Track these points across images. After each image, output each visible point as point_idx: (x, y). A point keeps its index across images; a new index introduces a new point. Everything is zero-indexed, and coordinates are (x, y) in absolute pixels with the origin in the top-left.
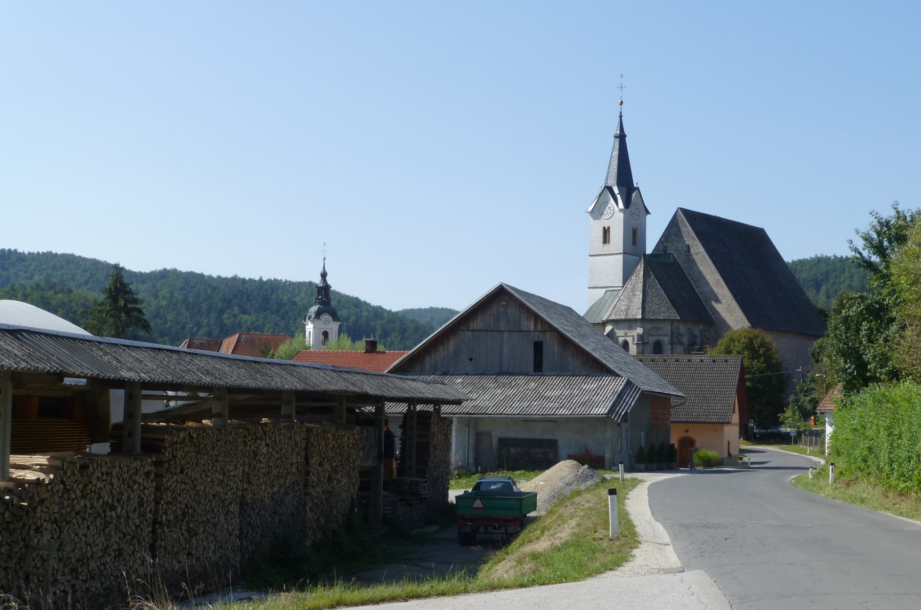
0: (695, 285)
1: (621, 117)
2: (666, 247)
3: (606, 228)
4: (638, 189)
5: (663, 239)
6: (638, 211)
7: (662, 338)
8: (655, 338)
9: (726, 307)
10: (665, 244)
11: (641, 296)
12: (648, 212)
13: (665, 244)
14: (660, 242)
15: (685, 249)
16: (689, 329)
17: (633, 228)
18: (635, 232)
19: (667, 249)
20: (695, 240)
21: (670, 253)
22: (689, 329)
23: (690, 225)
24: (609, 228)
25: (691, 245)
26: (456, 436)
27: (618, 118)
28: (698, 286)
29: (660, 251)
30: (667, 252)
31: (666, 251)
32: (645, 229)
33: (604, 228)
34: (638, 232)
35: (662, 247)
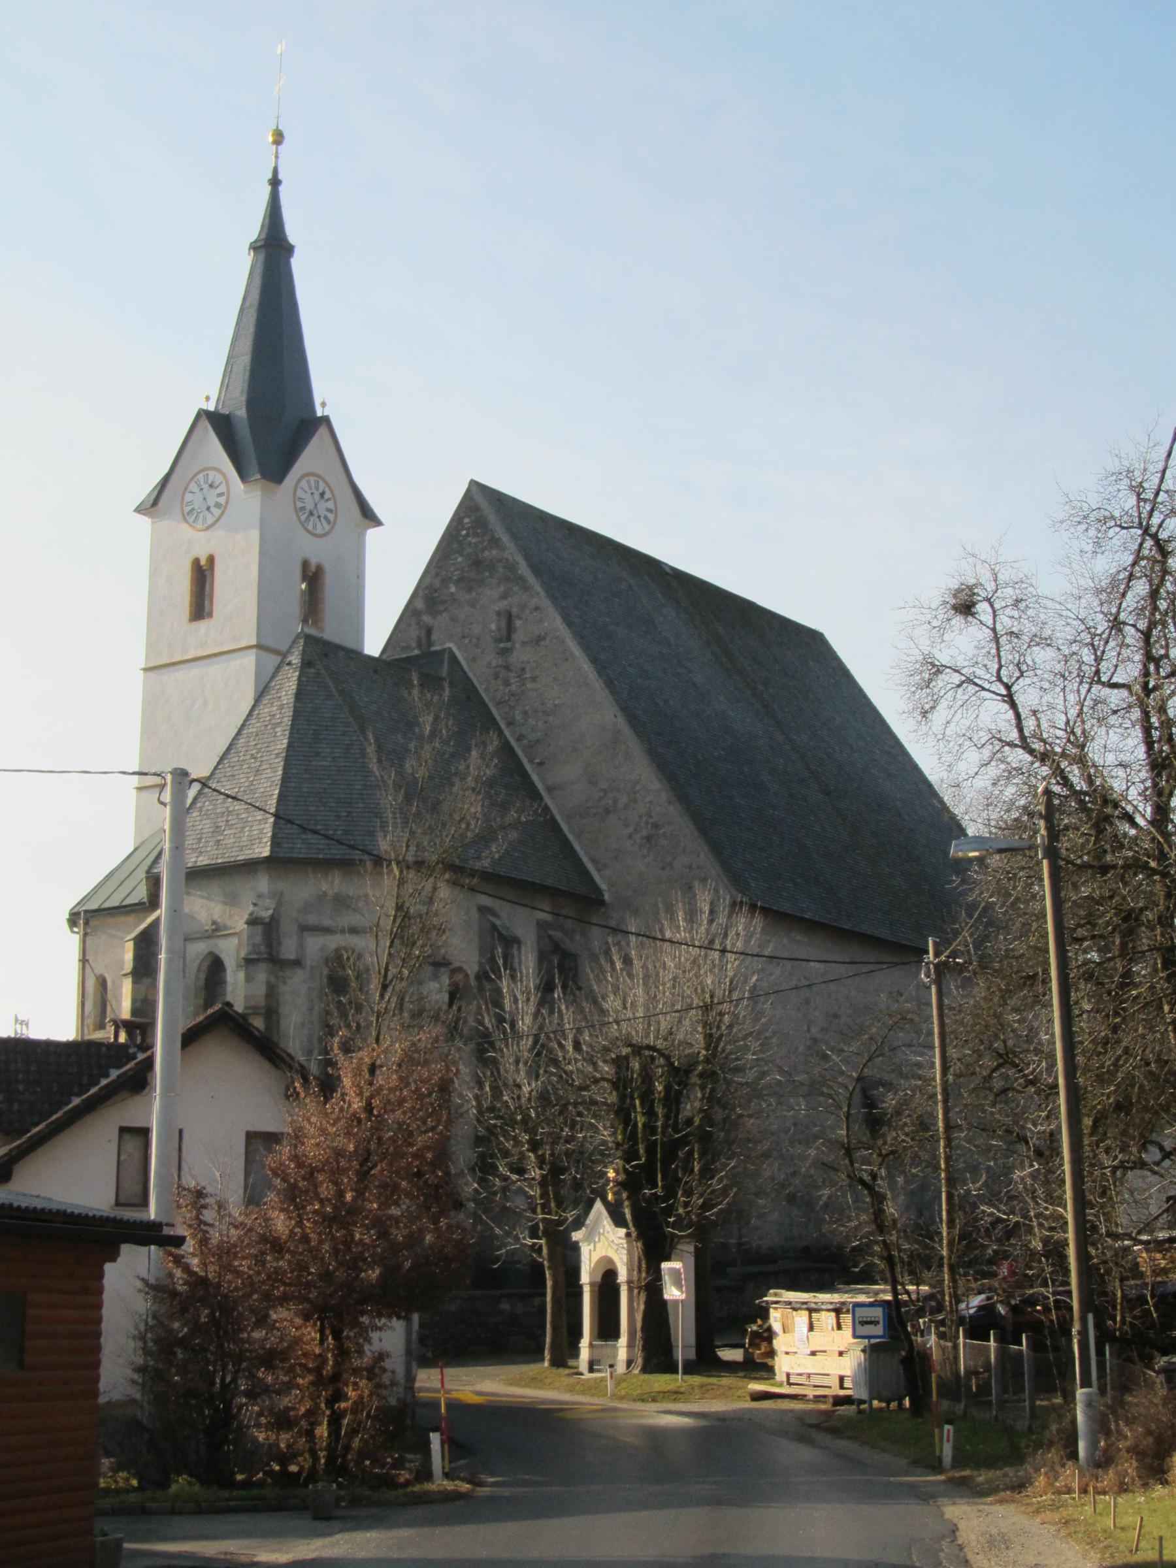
0: (531, 761)
1: (275, 182)
2: (429, 631)
3: (203, 562)
4: (326, 420)
5: (420, 604)
6: (331, 505)
7: (358, 942)
8: (333, 942)
9: (645, 833)
10: (426, 619)
11: (280, 773)
12: (369, 516)
13: (426, 619)
14: (410, 613)
15: (493, 627)
16: (482, 909)
17: (305, 564)
18: (313, 577)
19: (434, 637)
20: (525, 587)
21: (442, 652)
22: (482, 909)
23: (586, 648)
24: (211, 560)
25: (514, 610)
26: (792, 1411)
27: (268, 189)
28: (541, 764)
29: (408, 648)
30: (433, 649)
31: (430, 643)
32: (360, 576)
33: (196, 563)
34: (330, 583)
35: (414, 632)
